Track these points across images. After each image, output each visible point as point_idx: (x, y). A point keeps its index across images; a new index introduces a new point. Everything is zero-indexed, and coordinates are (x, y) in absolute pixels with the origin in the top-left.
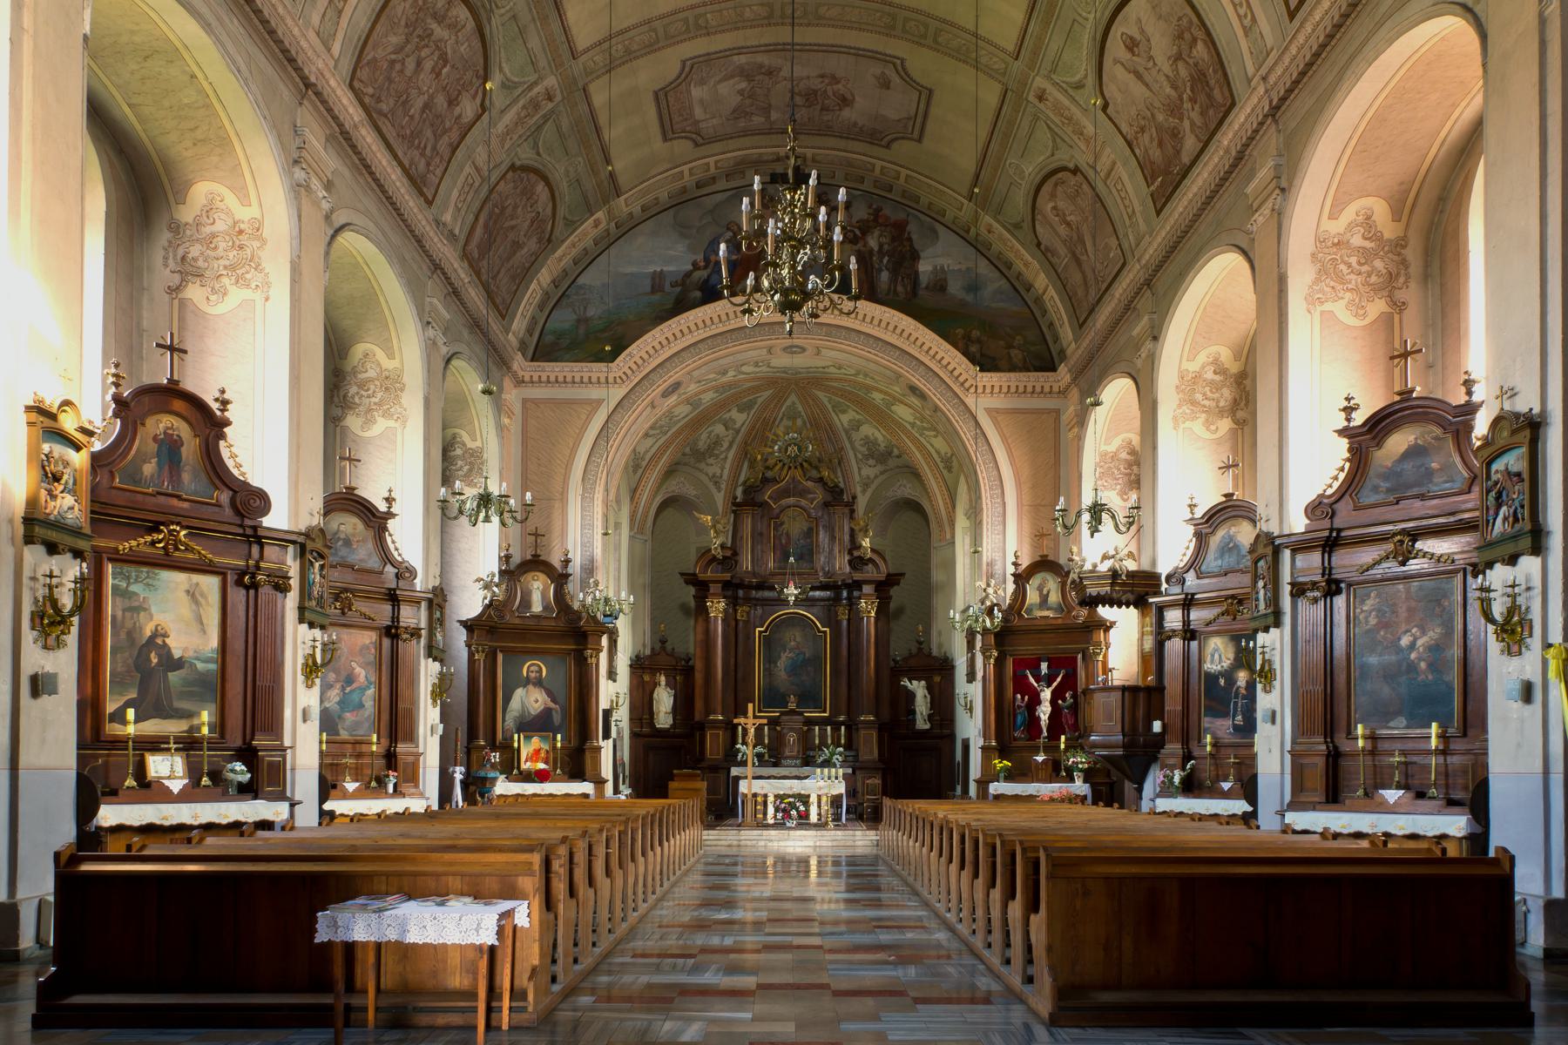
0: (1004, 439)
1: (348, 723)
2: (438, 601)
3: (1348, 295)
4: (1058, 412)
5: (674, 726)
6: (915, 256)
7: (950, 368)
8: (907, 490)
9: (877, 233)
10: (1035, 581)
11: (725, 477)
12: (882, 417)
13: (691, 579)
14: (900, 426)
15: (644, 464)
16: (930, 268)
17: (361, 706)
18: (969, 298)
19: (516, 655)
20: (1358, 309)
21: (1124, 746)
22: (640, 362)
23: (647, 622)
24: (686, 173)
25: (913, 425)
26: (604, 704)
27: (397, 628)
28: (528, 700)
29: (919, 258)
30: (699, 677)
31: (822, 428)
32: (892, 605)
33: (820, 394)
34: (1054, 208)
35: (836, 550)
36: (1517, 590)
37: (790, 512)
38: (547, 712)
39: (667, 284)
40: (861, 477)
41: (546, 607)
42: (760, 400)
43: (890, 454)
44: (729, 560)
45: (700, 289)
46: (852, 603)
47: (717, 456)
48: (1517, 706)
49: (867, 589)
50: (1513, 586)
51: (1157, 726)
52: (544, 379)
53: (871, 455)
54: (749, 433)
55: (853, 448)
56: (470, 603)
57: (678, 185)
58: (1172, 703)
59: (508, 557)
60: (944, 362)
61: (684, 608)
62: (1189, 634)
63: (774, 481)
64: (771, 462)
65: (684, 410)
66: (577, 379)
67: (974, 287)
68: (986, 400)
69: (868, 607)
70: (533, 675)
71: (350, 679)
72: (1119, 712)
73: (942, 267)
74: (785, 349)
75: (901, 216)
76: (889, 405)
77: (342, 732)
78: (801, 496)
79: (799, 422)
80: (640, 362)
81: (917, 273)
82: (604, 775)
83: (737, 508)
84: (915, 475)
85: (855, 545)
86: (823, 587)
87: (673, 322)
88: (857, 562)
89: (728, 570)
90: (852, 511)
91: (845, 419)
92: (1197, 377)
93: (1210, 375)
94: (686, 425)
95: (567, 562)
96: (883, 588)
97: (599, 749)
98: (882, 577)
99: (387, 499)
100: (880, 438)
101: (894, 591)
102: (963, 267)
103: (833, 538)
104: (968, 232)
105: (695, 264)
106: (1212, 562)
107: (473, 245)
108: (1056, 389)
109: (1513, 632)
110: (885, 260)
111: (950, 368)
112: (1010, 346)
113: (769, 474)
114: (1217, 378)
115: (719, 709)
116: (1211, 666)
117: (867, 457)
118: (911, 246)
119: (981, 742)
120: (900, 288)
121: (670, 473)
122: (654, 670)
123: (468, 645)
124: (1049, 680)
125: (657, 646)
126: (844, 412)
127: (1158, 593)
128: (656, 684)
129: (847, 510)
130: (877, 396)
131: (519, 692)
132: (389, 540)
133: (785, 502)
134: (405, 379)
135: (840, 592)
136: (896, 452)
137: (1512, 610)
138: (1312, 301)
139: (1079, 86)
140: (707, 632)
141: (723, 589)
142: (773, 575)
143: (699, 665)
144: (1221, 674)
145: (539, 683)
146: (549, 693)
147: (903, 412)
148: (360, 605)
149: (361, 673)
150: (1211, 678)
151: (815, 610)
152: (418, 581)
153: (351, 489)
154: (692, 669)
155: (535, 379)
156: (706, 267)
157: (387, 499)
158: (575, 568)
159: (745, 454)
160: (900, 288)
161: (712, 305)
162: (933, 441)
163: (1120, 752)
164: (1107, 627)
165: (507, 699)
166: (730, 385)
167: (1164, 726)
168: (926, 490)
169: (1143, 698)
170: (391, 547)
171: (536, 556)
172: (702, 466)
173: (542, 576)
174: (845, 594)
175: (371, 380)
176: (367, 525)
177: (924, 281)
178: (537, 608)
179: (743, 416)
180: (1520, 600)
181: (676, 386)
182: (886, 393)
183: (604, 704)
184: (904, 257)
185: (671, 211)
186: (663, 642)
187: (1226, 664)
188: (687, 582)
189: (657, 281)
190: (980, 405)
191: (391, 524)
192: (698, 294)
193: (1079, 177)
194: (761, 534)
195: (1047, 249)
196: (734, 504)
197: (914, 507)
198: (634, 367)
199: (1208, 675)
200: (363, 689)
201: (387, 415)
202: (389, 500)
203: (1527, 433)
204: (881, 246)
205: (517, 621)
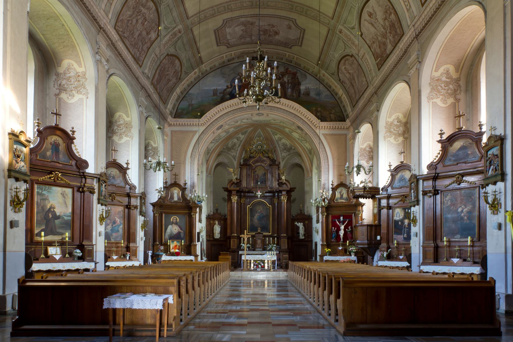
1: (114, 237)
2: (143, 197)
5: (220, 238)
6: (299, 84)
7: (311, 120)
8: (297, 160)
9: (287, 76)
10: (339, 190)
11: (237, 156)
12: (288, 136)
13: (226, 189)
14: (295, 139)
17: (118, 231)
18: (317, 98)
19: (169, 214)
21: (368, 244)
22: (209, 118)
25: (299, 139)
26: (197, 230)
27: (130, 206)
30: (229, 221)
31: (269, 140)
32: (292, 198)
33: (269, 129)
34: (345, 68)
36: (496, 193)
37: (258, 168)
38: (179, 233)
40: (282, 157)
41: (179, 199)
42: (249, 131)
44: (239, 183)
46: (279, 197)
47: (235, 149)
49: (284, 193)
50: (495, 192)
51: (379, 238)
52: (178, 124)
55: (279, 147)
56: (154, 197)
58: (384, 230)
59: (166, 182)
61: (224, 199)
62: (389, 207)
63: (253, 157)
65: (224, 134)
66: (189, 124)
67: (319, 94)
68: (323, 131)
69: (284, 199)
70: (174, 221)
71: (114, 222)
73: (308, 88)
74: (257, 114)
75: (295, 71)
78: (262, 162)
79: (261, 138)
80: (209, 118)
81: (300, 89)
82: (197, 254)
83: (241, 166)
84: (299, 155)
85: (280, 178)
86: (269, 192)
87: (220, 105)
88: (280, 184)
90: (279, 167)
91: (277, 137)
92: (392, 123)
94: (224, 139)
95: (185, 184)
96: (289, 192)
97: (196, 245)
98: (288, 189)
99: (127, 163)
100: (288, 143)
103: (272, 176)
104: (317, 76)
105: (227, 87)
106: (396, 184)
107: (155, 80)
108: (345, 127)
109: (495, 207)
110: (290, 85)
112: (330, 113)
114: (398, 124)
115: (235, 232)
116: (396, 218)
118: (298, 80)
119: (321, 243)
121: (219, 155)
122: (214, 219)
123: (153, 211)
126: (276, 135)
127: (379, 194)
128: (215, 224)
129: (277, 167)
132: (127, 177)
133: (257, 164)
135: (275, 194)
136: (293, 148)
137: (495, 200)
138: (429, 98)
139: (353, 28)
141: (237, 193)
142: (253, 188)
143: (229, 218)
144: (399, 221)
145: (176, 223)
146: (180, 227)
147: (295, 135)
149: (118, 220)
150: (396, 222)
151: (267, 200)
152: (137, 190)
153: (115, 160)
154: (226, 219)
155: (175, 124)
156: (231, 88)
157: (127, 163)
158: (188, 186)
159: (244, 148)
160: (294, 94)
162: (305, 144)
163: (366, 246)
164: (362, 205)
165: (166, 229)
166: (239, 126)
167: (381, 238)
168: (303, 160)
169: (374, 228)
170: (128, 179)
171: (175, 182)
172: (230, 152)
173: (177, 189)
174: (276, 194)
175: (121, 124)
176: (120, 172)
177: (302, 92)
178: (176, 199)
179: (243, 136)
180: (497, 196)
181: (221, 126)
182: (290, 129)
183: (197, 230)
184: (296, 85)
185: (220, 69)
186: (217, 210)
187: (401, 217)
188: (225, 191)
189: (215, 92)
190: (321, 132)
191: (128, 171)
192: (228, 96)
193: (353, 58)
194: (249, 175)
195: (343, 82)
196: (240, 165)
197: (299, 166)
199: (395, 221)
200: (119, 226)
202: (127, 164)
203: (500, 142)
204: (288, 80)
205: (169, 203)
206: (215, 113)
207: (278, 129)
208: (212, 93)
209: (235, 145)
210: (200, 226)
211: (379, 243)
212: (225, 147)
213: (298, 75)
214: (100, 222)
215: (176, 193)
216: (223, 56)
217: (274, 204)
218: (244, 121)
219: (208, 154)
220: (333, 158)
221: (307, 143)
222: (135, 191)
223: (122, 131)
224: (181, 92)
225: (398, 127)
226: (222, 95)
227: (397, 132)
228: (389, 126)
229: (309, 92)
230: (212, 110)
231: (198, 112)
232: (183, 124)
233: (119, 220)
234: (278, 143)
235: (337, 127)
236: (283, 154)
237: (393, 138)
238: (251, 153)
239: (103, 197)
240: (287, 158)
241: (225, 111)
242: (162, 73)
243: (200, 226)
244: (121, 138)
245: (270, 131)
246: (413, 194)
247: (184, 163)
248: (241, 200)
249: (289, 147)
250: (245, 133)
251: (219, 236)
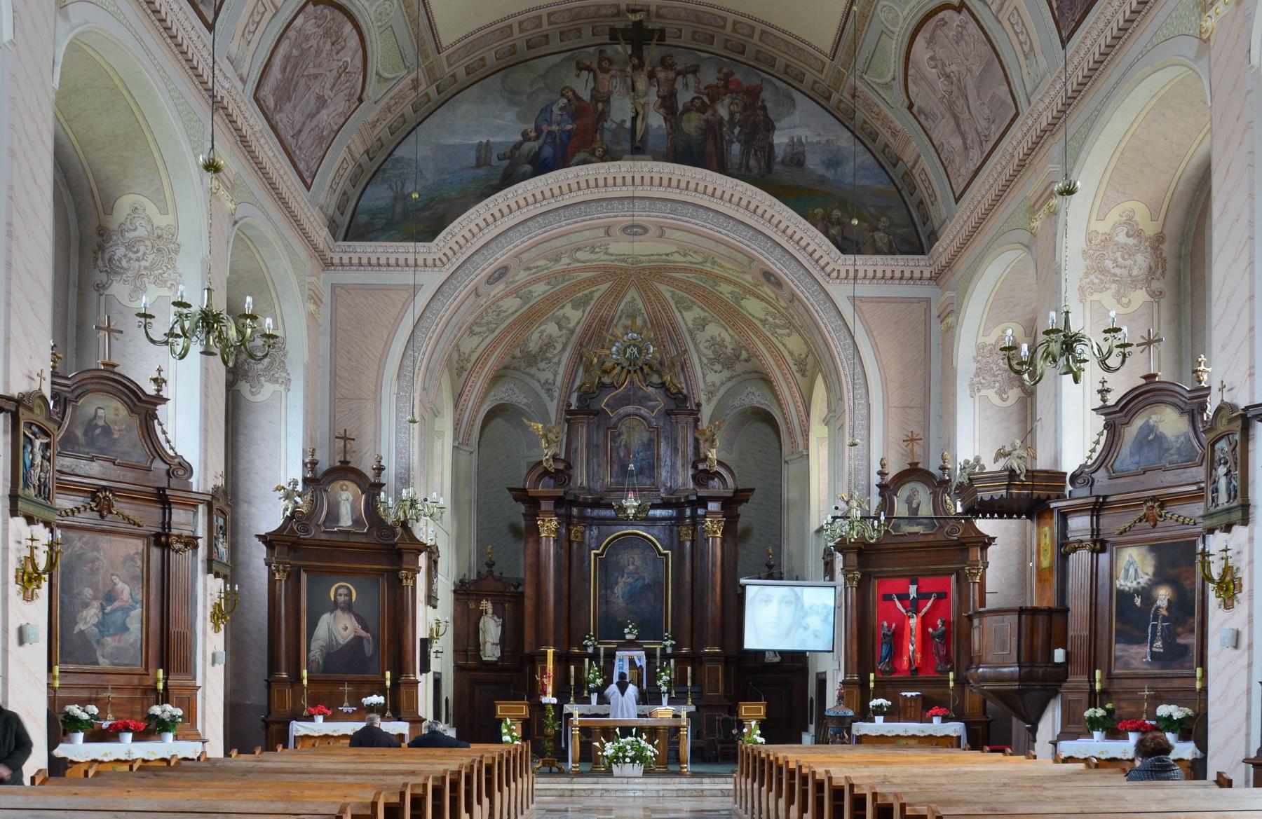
0: (869, 332)
1: (108, 649)
2: (226, 503)
3: (1114, 286)
4: (928, 301)
5: (501, 658)
6: (770, 127)
7: (810, 249)
8: (756, 397)
9: (727, 101)
10: (904, 492)
11: (558, 383)
12: (731, 314)
13: (520, 495)
14: (750, 324)
15: (470, 365)
16: (785, 140)
17: (124, 629)
18: (830, 174)
19: (323, 575)
20: (1001, 393)
21: (1021, 679)
22: (462, 241)
23: (473, 543)
24: (516, 28)
25: (764, 322)
26: (421, 633)
27: (168, 536)
28: (337, 628)
29: (774, 128)
30: (529, 604)
31: (663, 328)
32: (740, 526)
33: (664, 289)
34: (932, 58)
35: (679, 463)
36: (1229, 553)
37: (627, 422)
38: (358, 640)
39: (494, 157)
40: (706, 383)
41: (357, 522)
42: (596, 295)
43: (738, 357)
44: (562, 474)
45: (530, 163)
46: (696, 521)
47: (550, 360)
48: (1231, 653)
49: (713, 506)
50: (1226, 550)
51: (1059, 656)
52: (355, 261)
53: (717, 359)
54: (585, 332)
55: (698, 351)
56: (268, 514)
57: (508, 42)
58: (1077, 624)
59: (314, 463)
60: (803, 243)
61: (515, 530)
62: (1099, 544)
63: (612, 386)
64: (608, 365)
65: (511, 304)
66: (392, 261)
67: (834, 162)
68: (851, 292)
69: (713, 526)
70: (341, 599)
71: (110, 597)
72: (1015, 638)
73: (800, 140)
74: (624, 229)
75: (755, 81)
76: (738, 299)
77: (101, 660)
78: (641, 403)
79: (639, 321)
80: (462, 241)
81: (771, 146)
82: (421, 713)
83: (571, 417)
84: (766, 380)
85: (699, 458)
86: (665, 505)
87: (499, 196)
88: (703, 477)
89: (562, 486)
90: (697, 420)
91: (689, 316)
92: (1108, 238)
93: (1121, 238)
94: (514, 323)
95: (380, 469)
96: (731, 504)
97: (416, 683)
98: (729, 493)
99: (155, 380)
100: (728, 339)
101: (742, 509)
102: (823, 140)
103: (675, 450)
104: (828, 99)
105: (525, 135)
106: (1126, 456)
107: (267, 90)
108: (927, 274)
109: (1228, 589)
110: (737, 130)
111: (810, 249)
112: (876, 229)
113: (606, 380)
114: (1131, 241)
115: (551, 640)
116: (1123, 583)
117: (712, 361)
118: (766, 115)
119: (841, 677)
120: (752, 163)
121: (498, 378)
122: (479, 597)
123: (268, 564)
124: (915, 606)
125: (484, 570)
126: (688, 308)
127: (1060, 497)
128: (482, 613)
129: (691, 419)
130: (725, 289)
131: (326, 619)
132: (158, 429)
133: (622, 411)
134: (181, 238)
135: (684, 507)
136: (744, 355)
137: (1227, 570)
138: (974, 388)
139: (887, 86)
140: (537, 554)
141: (556, 506)
142: (610, 491)
143: (528, 591)
144: (1136, 591)
145: (348, 608)
146: (360, 620)
147: (753, 307)
148: (122, 507)
149: (125, 590)
150: (1124, 598)
151: (655, 530)
152: (193, 480)
153: (110, 366)
154: (522, 595)
155: (346, 261)
156: (537, 138)
157: (155, 380)
158: (389, 477)
159: (579, 357)
160: (752, 163)
161: (543, 177)
162: (786, 340)
163: (1015, 686)
164: (985, 542)
165: (312, 626)
166: (565, 273)
167: (1067, 655)
168: (779, 401)
169: (1042, 623)
170: (161, 437)
171: (345, 462)
172: (533, 371)
173: (352, 486)
174: (688, 512)
175: (140, 240)
176: (132, 409)
177: (779, 153)
178: (346, 521)
179: (578, 314)
180: (1230, 562)
181: (503, 271)
182: (736, 284)
183: (421, 633)
184: (758, 127)
185: (500, 75)
186: (491, 565)
187: (1144, 580)
188: (516, 500)
189: (483, 153)
190: (840, 292)
191: (160, 410)
192: (528, 168)
193: (964, 15)
194: (597, 446)
195: (921, 111)
196: (569, 412)
197: (766, 418)
198: (456, 247)
199: (1121, 593)
200: (127, 610)
201: (273, 380)
202: (159, 382)
203: (1239, 422)
204: (732, 114)
205: (323, 537)
206: (482, 224)
207: (696, 286)
208: (471, 158)
209: (550, 344)
210: (432, 618)
211: (1061, 672)
212: (517, 352)
213: (766, 94)
214: (25, 589)
215: (348, 500)
216: (510, 27)
217: (681, 544)
218: (581, 255)
219: (459, 375)
220: (885, 384)
221: (795, 336)
222: (190, 485)
223: (144, 264)
224: (367, 152)
225: (1128, 252)
226: (506, 163)
227: (1125, 272)
228: (1099, 247)
229: (803, 153)
230: (471, 213)
231: (426, 222)
232: (374, 261)
233: (127, 589)
234: (693, 339)
235: (898, 274)
236: (713, 378)
237: (1111, 292)
238: (605, 372)
239: (32, 492)
240: (722, 391)
241: (518, 217)
242: (295, 67)
243: (432, 618)
244: (138, 290)
245: (668, 295)
246: (1223, 483)
247: (377, 399)
248: (569, 531)
249: (729, 351)
250: (586, 303)
251: (498, 653)
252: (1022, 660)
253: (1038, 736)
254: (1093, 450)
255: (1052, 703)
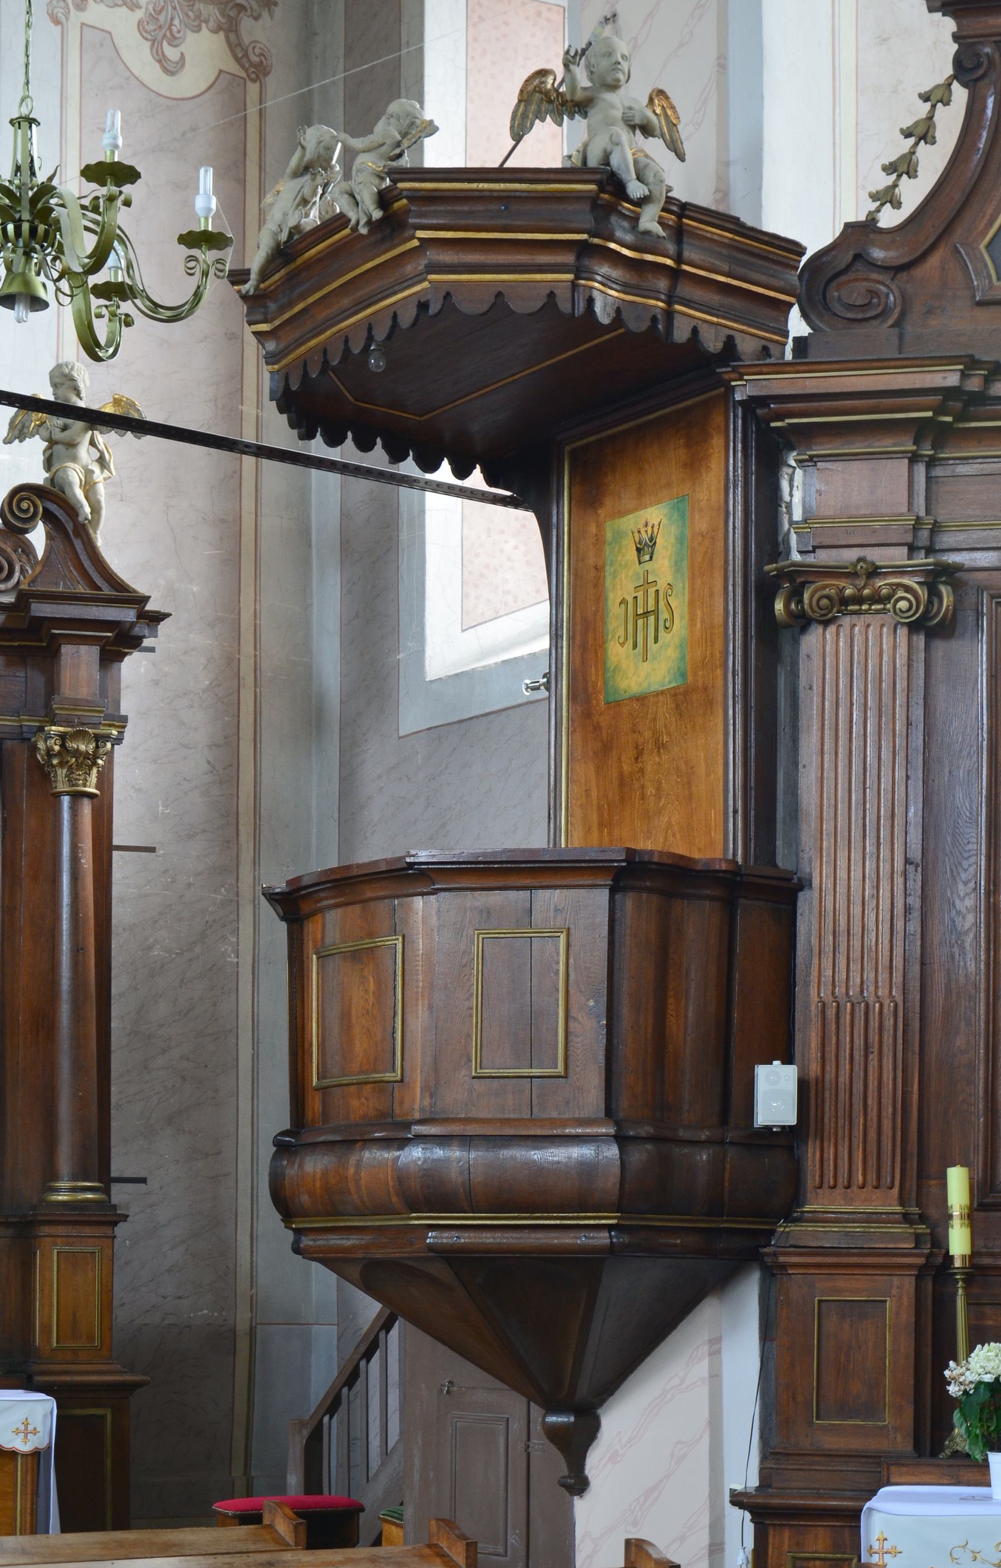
51: (775, 1094)
252: (623, 1103)
253: (596, 1462)
254: (903, 167)
255: (708, 1314)
